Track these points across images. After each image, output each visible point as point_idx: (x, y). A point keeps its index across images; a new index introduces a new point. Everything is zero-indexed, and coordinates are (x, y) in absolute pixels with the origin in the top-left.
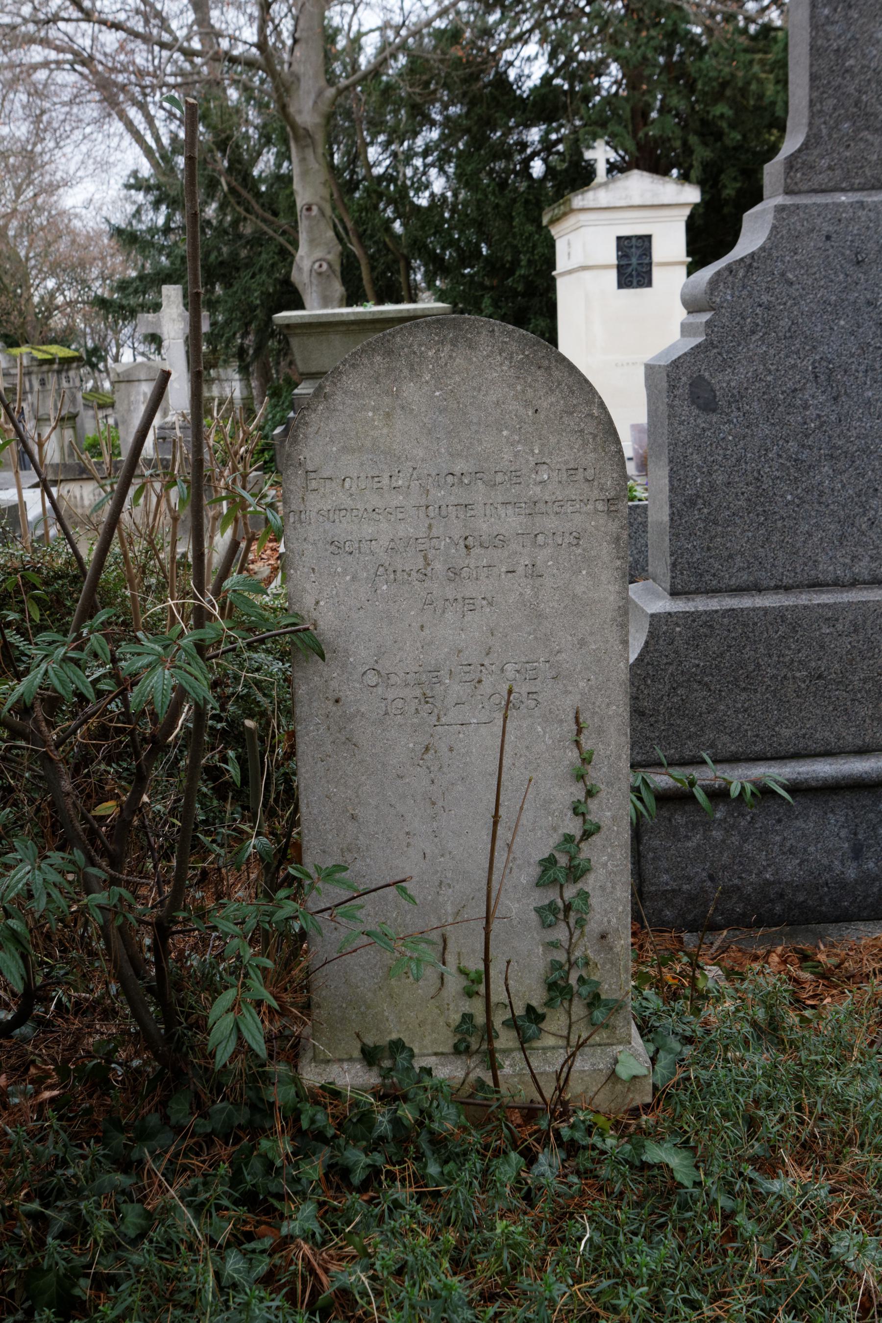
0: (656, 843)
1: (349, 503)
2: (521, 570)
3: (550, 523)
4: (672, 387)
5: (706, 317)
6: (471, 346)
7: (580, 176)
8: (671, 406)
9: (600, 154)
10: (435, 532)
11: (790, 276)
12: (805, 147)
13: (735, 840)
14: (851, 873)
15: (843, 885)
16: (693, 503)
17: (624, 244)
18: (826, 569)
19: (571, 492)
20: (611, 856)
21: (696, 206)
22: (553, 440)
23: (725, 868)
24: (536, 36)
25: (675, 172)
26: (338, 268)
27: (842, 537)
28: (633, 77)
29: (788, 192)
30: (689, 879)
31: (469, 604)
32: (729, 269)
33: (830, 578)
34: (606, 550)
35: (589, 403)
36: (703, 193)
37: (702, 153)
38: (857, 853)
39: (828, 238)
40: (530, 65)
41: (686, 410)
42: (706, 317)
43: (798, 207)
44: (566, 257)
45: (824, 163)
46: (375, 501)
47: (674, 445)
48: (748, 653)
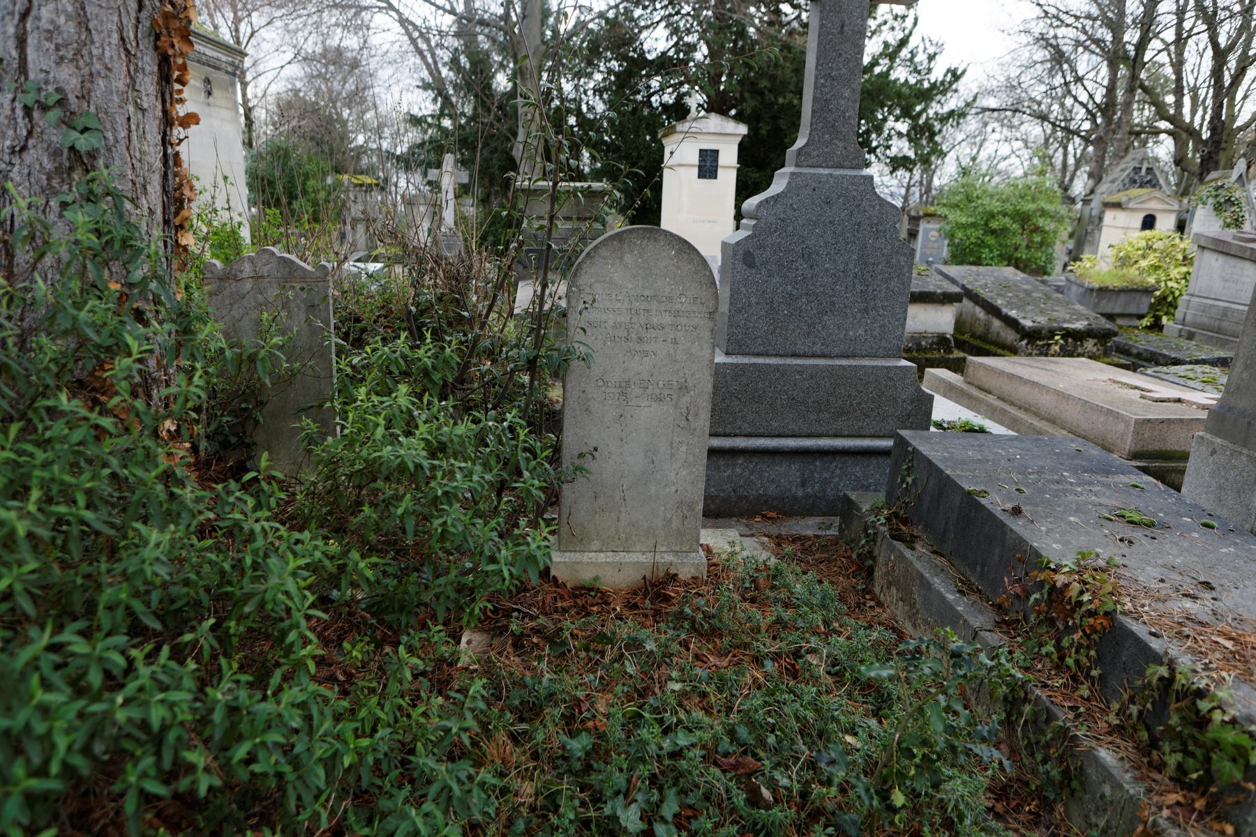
3: (683, 321)
6: (656, 240)
7: (679, 111)
9: (696, 99)
12: (807, 144)
14: (800, 494)
15: (795, 498)
17: (703, 153)
18: (800, 348)
19: (694, 308)
24: (663, 24)
27: (809, 334)
29: (797, 165)
30: (723, 491)
31: (646, 354)
32: (767, 200)
37: (750, 105)
40: (656, 42)
41: (740, 266)
45: (815, 153)
46: (608, 305)
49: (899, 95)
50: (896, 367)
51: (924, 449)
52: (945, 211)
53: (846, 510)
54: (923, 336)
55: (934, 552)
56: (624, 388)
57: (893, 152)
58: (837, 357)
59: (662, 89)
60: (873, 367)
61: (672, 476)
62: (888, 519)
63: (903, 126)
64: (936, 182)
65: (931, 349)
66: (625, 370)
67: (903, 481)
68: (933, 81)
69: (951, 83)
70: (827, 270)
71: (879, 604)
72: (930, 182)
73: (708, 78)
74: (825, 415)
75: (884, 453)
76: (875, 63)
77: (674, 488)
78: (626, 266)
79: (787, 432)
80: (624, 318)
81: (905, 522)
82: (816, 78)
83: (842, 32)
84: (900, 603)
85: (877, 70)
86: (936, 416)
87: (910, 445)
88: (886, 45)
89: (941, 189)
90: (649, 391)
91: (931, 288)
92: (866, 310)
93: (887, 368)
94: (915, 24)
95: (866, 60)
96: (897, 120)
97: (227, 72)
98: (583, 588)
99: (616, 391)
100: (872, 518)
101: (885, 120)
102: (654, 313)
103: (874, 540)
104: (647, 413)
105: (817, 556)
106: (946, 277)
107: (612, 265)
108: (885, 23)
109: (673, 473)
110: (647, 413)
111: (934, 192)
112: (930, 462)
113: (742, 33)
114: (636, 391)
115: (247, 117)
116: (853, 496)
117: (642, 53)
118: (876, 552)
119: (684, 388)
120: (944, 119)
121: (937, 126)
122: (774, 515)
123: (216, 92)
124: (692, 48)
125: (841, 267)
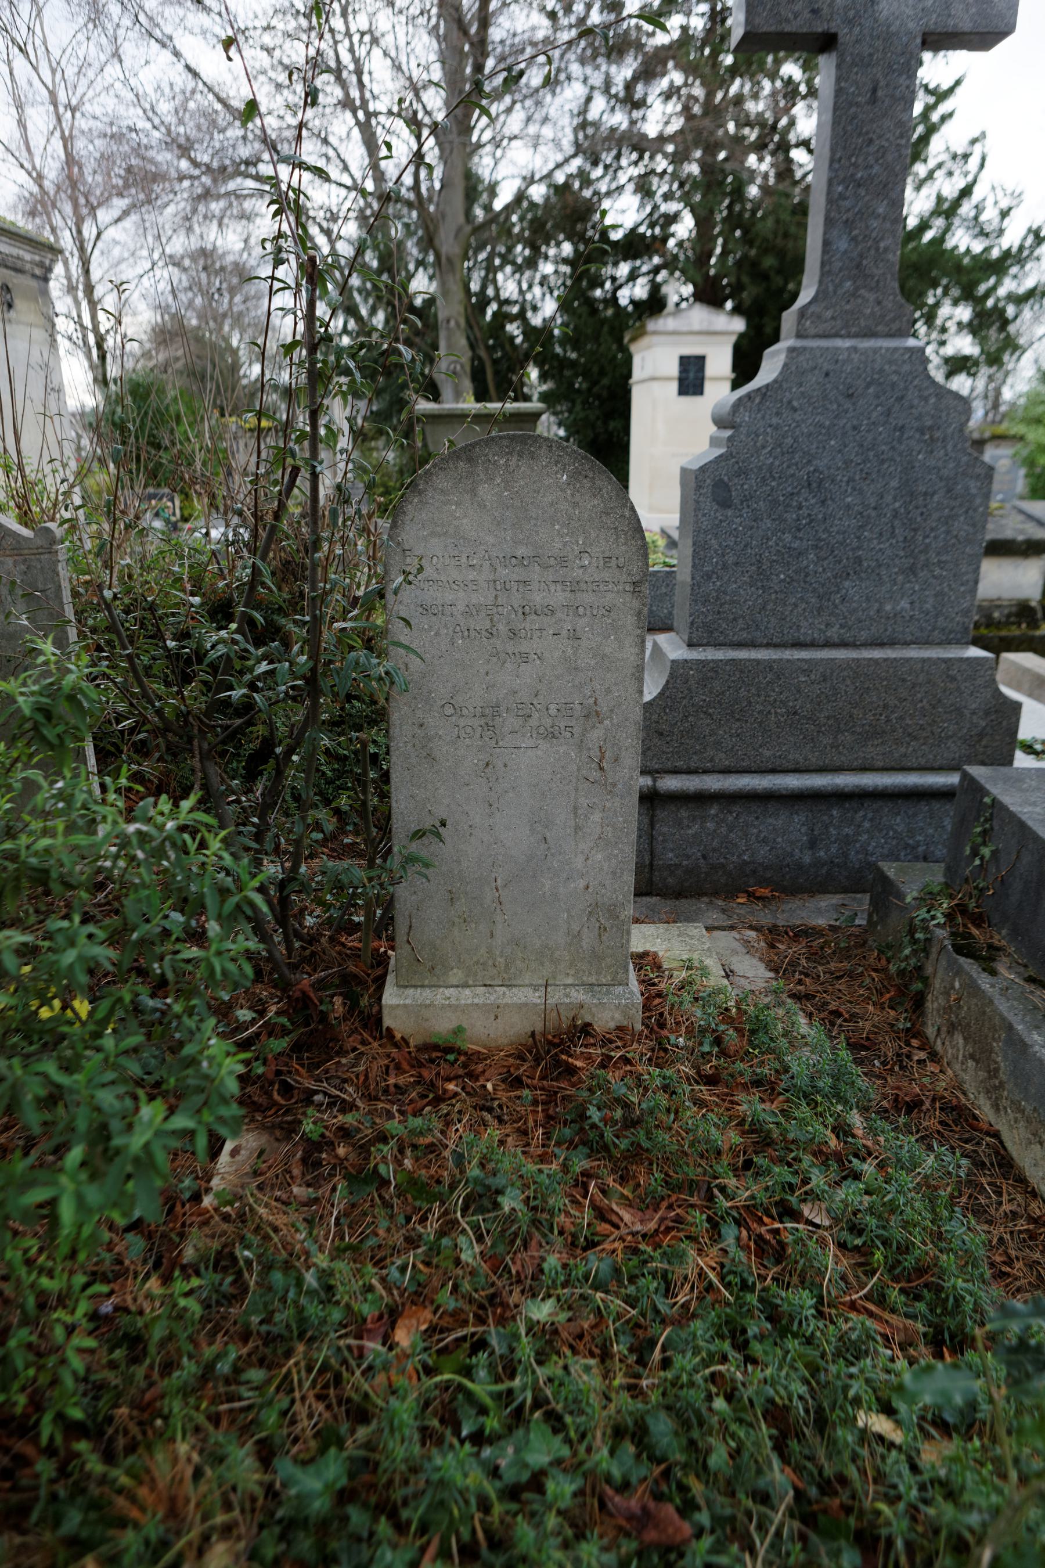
0: (665, 829)
1: (435, 576)
2: (564, 633)
3: (587, 598)
4: (699, 487)
5: (728, 433)
6: (533, 456)
7: (654, 304)
8: (697, 502)
10: (500, 602)
11: (795, 404)
13: (724, 830)
14: (807, 859)
16: (710, 578)
18: (806, 632)
19: (606, 575)
20: (622, 851)
21: (741, 336)
22: (593, 534)
23: (714, 850)
25: (729, 305)
26: (468, 369)
27: (820, 609)
28: (703, 223)
29: (799, 336)
30: (688, 857)
31: (525, 658)
33: (808, 639)
34: (630, 621)
35: (624, 506)
36: (748, 325)
38: (813, 844)
39: (827, 375)
40: (624, 213)
42: (728, 433)
43: (805, 349)
44: (640, 369)
46: (455, 575)
47: (697, 531)
48: (743, 692)
49: (958, 268)
50: (962, 660)
51: (1011, 800)
52: (1020, 429)
53: (883, 893)
54: (995, 604)
55: (1030, 980)
56: (490, 717)
57: (949, 350)
58: (866, 645)
59: (632, 277)
60: (924, 660)
61: (579, 862)
62: (949, 916)
63: (964, 313)
64: (1007, 394)
65: (1008, 624)
66: (490, 687)
67: (975, 853)
68: (1005, 247)
69: (1033, 248)
70: (848, 507)
71: (934, 1057)
72: (998, 393)
73: (694, 264)
74: (848, 738)
75: (945, 794)
76: (924, 226)
77: (582, 883)
78: (482, 506)
79: (786, 765)
80: (483, 597)
81: (978, 920)
82: (830, 183)
83: (873, 100)
84: (970, 1063)
85: (928, 236)
86: (1024, 733)
87: (987, 793)
88: (940, 199)
89: (1013, 405)
90: (534, 722)
91: (1008, 534)
92: (912, 570)
93: (946, 661)
94: (982, 166)
95: (912, 222)
96: (955, 303)
97: (34, 276)
98: (436, 1047)
99: (476, 722)
100: (923, 913)
101: (937, 305)
102: (535, 586)
103: (926, 951)
104: (530, 759)
105: (833, 966)
106: (1030, 517)
107: (458, 504)
108: (940, 166)
109: (580, 859)
110: (530, 759)
111: (1003, 409)
112: (1022, 825)
113: (738, 192)
114: (512, 722)
115: (100, 346)
116: (890, 870)
117: (604, 233)
118: (929, 970)
119: (592, 715)
120: (1020, 300)
121: (1011, 310)
122: (765, 892)
123: (18, 303)
124: (673, 219)
125: (872, 501)
